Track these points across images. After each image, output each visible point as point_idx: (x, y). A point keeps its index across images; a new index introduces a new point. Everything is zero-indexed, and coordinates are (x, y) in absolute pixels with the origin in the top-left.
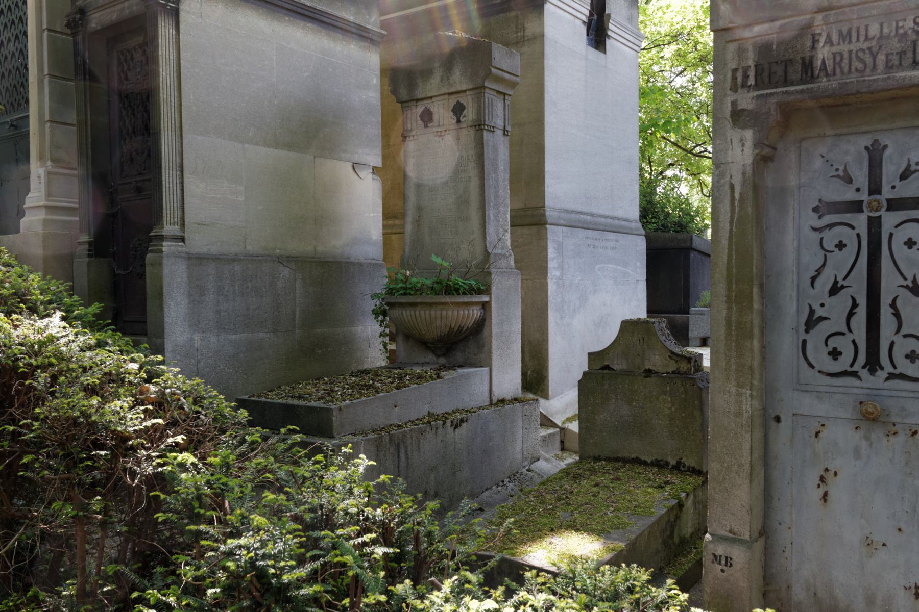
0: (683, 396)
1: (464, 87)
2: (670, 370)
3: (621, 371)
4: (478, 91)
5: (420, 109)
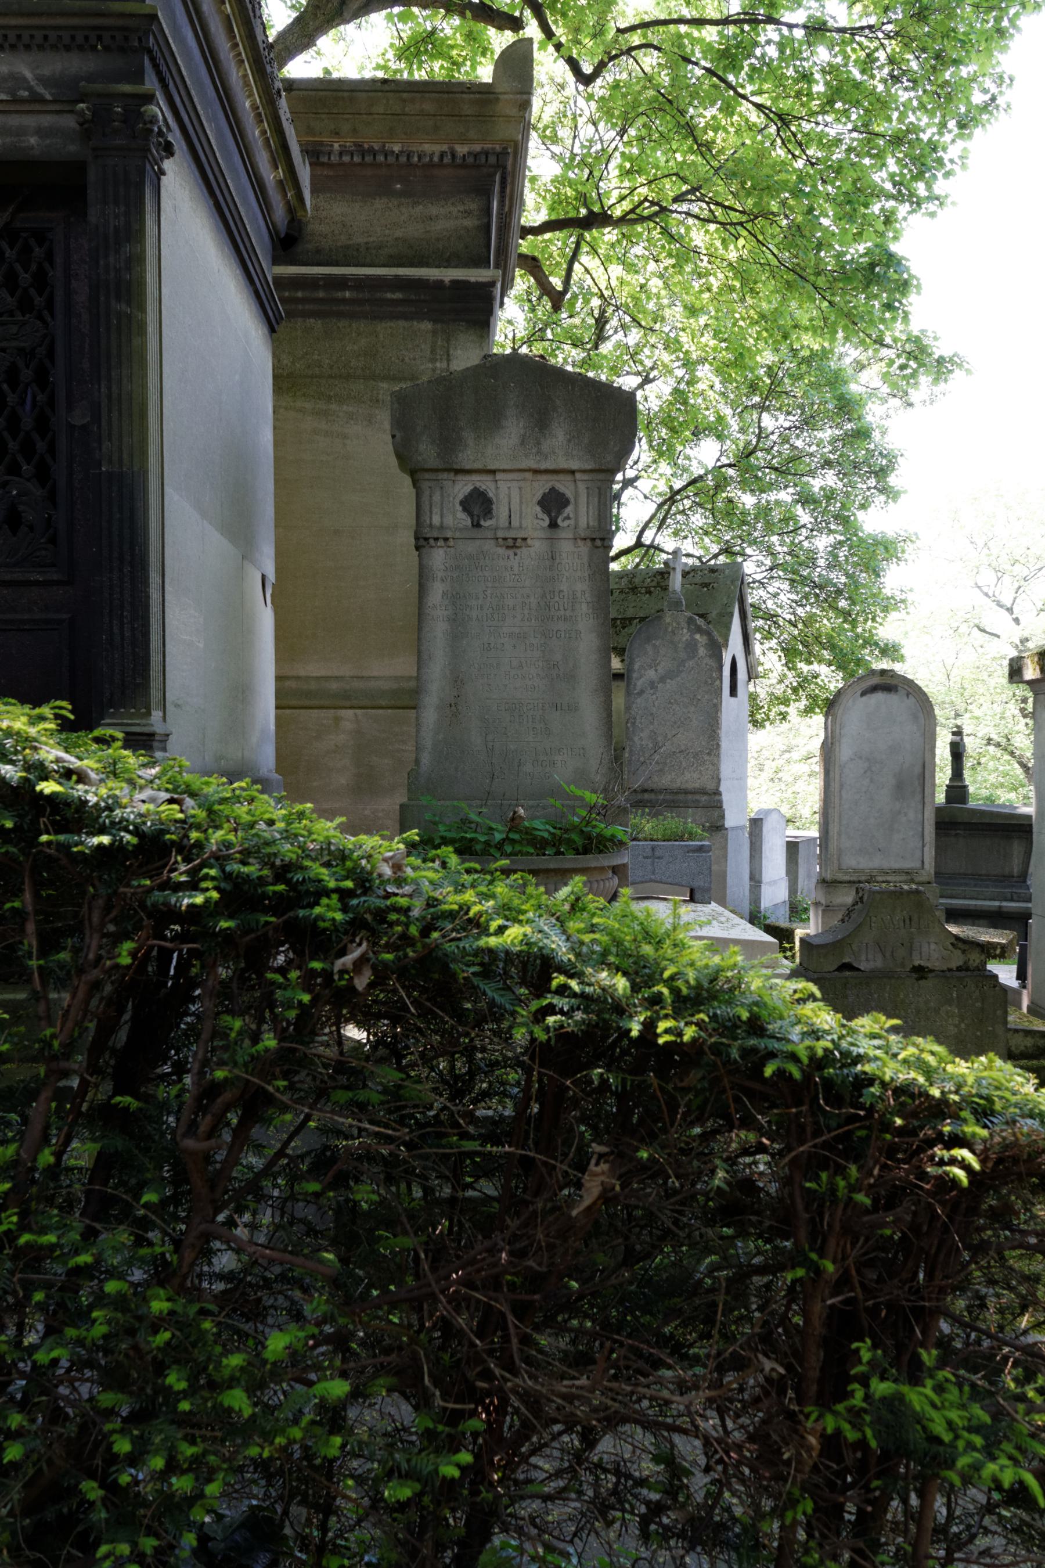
0: (978, 1005)
1: (574, 465)
2: (954, 965)
3: (872, 971)
4: (601, 476)
5: (463, 487)
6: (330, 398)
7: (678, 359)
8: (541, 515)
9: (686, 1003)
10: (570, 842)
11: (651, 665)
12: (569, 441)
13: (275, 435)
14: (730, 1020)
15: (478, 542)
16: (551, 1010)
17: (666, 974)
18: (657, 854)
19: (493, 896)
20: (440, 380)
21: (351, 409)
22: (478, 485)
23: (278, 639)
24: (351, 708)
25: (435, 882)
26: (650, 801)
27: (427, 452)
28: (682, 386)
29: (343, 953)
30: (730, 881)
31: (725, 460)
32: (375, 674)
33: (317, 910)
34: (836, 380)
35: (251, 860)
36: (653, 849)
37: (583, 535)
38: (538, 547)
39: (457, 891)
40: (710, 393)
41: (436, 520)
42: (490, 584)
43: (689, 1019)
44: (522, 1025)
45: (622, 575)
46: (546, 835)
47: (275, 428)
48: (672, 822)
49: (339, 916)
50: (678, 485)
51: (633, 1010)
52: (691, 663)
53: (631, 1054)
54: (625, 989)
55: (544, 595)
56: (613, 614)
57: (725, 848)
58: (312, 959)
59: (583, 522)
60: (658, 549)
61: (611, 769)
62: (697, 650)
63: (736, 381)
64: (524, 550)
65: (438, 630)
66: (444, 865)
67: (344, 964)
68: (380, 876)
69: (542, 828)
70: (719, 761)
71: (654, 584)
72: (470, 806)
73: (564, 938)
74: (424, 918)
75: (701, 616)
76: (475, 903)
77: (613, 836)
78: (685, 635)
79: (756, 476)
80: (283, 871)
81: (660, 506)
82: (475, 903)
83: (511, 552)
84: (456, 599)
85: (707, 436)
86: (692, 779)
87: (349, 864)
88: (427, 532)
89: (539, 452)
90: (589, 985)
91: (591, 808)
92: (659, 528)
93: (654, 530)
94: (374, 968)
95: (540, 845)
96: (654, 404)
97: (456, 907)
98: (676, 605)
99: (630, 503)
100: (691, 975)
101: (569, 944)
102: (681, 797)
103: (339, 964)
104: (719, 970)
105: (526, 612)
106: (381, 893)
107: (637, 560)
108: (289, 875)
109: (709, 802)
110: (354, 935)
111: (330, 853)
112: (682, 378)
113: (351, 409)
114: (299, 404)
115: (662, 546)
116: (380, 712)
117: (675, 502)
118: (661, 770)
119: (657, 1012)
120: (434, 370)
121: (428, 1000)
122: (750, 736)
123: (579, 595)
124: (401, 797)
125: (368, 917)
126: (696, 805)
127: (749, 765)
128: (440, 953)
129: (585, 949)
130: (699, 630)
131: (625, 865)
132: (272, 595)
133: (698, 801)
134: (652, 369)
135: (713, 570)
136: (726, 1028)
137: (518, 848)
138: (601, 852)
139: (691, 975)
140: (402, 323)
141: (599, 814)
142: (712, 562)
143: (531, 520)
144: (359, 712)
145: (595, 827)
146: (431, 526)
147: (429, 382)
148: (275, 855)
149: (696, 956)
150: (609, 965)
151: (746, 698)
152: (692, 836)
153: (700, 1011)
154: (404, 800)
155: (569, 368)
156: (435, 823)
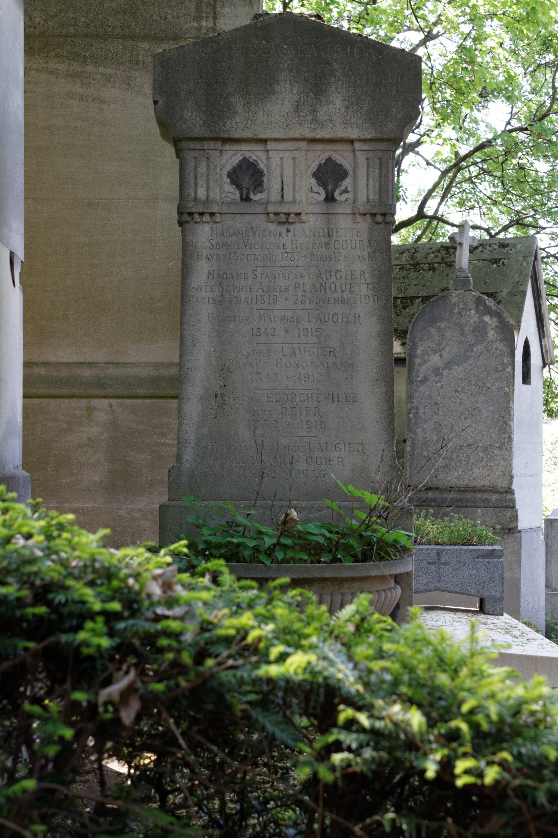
1: (353, 134)
4: (383, 146)
5: (231, 158)
6: (85, 58)
7: (464, 14)
8: (316, 188)
9: (488, 740)
10: (347, 547)
11: (435, 349)
12: (347, 107)
13: (26, 99)
14: (536, 759)
15: (247, 217)
16: (338, 747)
17: (465, 708)
18: (443, 559)
19: (272, 618)
20: (206, 42)
21: (108, 71)
22: (247, 155)
23: (28, 320)
24: (105, 397)
25: (211, 603)
26: (435, 500)
27: (192, 120)
28: (469, 43)
29: (108, 682)
30: (523, 589)
31: (515, 124)
32: (133, 359)
33: (82, 636)
35: (10, 579)
36: (438, 554)
37: (362, 210)
38: (313, 222)
39: (234, 614)
40: (500, 50)
41: (201, 193)
43: (491, 758)
44: (306, 763)
45: (402, 250)
46: (321, 540)
47: (25, 91)
48: (460, 524)
49: (105, 642)
50: (464, 150)
51: (427, 747)
52: (479, 348)
53: (422, 794)
54: (420, 726)
55: (319, 276)
56: (394, 293)
57: (518, 552)
58: (75, 688)
59: (362, 196)
60: (442, 220)
61: (393, 467)
62: (486, 333)
63: (528, 38)
64: (298, 226)
65: (203, 313)
66: (215, 581)
67: (110, 695)
68: (149, 596)
69: (316, 532)
70: (511, 456)
71: (438, 260)
72: (236, 507)
73: (351, 665)
74: (197, 643)
75: (491, 295)
76: (253, 628)
77: (395, 541)
78: (473, 317)
79: (550, 141)
80: (43, 592)
81: (444, 173)
82: (253, 628)
83: (283, 229)
84: (223, 279)
85: (497, 97)
86: (480, 476)
87: (115, 583)
88: (191, 206)
90: (381, 718)
91: (372, 511)
92: (443, 198)
93: (438, 200)
94: (142, 699)
95: (315, 551)
96: (438, 63)
97: (232, 632)
98: (463, 284)
99: (411, 170)
100: (493, 710)
101: (356, 673)
102: (469, 496)
103: (105, 694)
104: (521, 703)
105: (300, 294)
106: (150, 615)
107: (419, 232)
108: (51, 596)
109: (500, 501)
110: (121, 662)
111: (95, 571)
112: (469, 34)
113: (108, 71)
114: (51, 65)
115: (447, 217)
116: (138, 401)
117: (460, 169)
118: (447, 466)
119: (455, 750)
120: (199, 29)
121: (199, 732)
122: (545, 426)
123: (358, 276)
124: (161, 497)
125: (136, 642)
126: (486, 505)
127: (544, 458)
128: (215, 683)
129: (373, 678)
130: (488, 311)
131: (408, 574)
132: (21, 274)
133: (487, 500)
134: (435, 24)
135: (503, 245)
136: (530, 767)
137: (290, 554)
138: (382, 559)
139: (493, 710)
141: (379, 517)
142: (501, 236)
143: (306, 194)
144: (114, 401)
145: (375, 531)
146: (195, 199)
147: (195, 43)
148: (36, 574)
149: (497, 687)
150: (400, 696)
151: (541, 386)
152: (481, 540)
153: (502, 750)
154: (164, 499)
155: (345, 25)
156: (199, 527)
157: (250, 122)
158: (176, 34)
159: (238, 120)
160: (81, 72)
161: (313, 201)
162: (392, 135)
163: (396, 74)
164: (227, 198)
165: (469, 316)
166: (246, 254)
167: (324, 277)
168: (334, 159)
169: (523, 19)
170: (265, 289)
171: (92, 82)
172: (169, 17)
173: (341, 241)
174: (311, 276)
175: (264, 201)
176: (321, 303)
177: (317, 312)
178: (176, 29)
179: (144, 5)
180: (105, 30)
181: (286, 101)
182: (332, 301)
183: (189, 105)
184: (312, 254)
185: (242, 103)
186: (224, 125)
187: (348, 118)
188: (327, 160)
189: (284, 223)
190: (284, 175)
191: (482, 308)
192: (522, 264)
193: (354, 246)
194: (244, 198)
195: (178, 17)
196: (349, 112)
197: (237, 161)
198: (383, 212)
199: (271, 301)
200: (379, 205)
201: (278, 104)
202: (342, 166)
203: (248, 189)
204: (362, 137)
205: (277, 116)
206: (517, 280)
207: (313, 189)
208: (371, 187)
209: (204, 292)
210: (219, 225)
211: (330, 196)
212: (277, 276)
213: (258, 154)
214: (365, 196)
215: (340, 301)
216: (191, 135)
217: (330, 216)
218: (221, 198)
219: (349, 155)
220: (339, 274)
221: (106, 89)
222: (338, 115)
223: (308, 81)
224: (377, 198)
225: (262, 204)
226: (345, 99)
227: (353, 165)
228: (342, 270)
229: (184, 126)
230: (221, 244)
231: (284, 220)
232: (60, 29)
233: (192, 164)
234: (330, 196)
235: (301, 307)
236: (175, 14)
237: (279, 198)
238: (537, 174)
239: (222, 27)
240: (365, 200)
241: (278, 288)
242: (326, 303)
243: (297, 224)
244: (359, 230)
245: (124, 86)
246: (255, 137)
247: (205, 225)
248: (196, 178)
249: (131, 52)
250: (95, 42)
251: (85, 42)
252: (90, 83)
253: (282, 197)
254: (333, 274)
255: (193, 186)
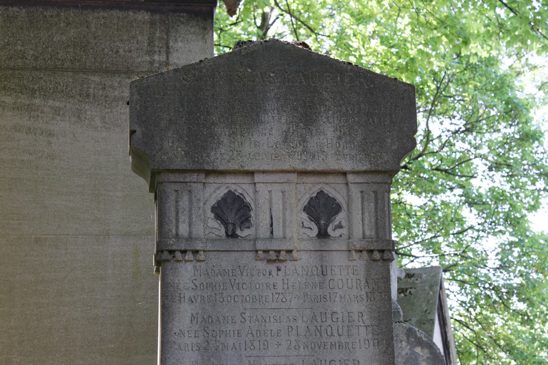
1: (347, 165)
4: (379, 178)
5: (214, 191)
6: (33, 91)
8: (308, 223)
12: (340, 138)
15: (234, 255)
21: (57, 104)
22: (233, 188)
34: (501, 87)
37: (358, 247)
38: (305, 260)
41: (184, 229)
42: (248, 306)
55: (314, 318)
59: (358, 232)
64: (289, 264)
83: (273, 267)
84: (208, 324)
88: (172, 244)
89: (305, 151)
105: (293, 338)
113: (57, 104)
120: (152, 63)
123: (356, 317)
140: (116, 13)
143: (297, 230)
157: (235, 153)
158: (128, 68)
159: (223, 151)
160: (29, 105)
161: (305, 237)
162: (387, 167)
163: (389, 104)
164: (211, 234)
165: (401, 347)
166: (233, 295)
167: (319, 320)
168: (326, 192)
169: (402, 68)
170: (254, 333)
171: (40, 115)
172: (121, 50)
173: (336, 280)
174: (305, 319)
175: (252, 237)
176: (317, 348)
177: (313, 358)
178: (128, 63)
179: (95, 38)
180: (55, 63)
181: (274, 131)
182: (329, 346)
183: (170, 135)
184: (305, 295)
185: (227, 133)
186: (208, 156)
187: (341, 149)
188: (318, 193)
189: (274, 261)
190: (273, 209)
191: (413, 340)
192: (428, 294)
193: (350, 286)
194: (230, 234)
195: (130, 51)
196: (341, 143)
197: (222, 195)
198: (380, 248)
199: (262, 347)
200: (376, 241)
201: (265, 134)
202: (335, 200)
203: (234, 225)
204: (356, 169)
205: (265, 147)
206: (425, 309)
207: (305, 224)
208: (366, 222)
209: (187, 337)
210: (202, 263)
211: (323, 232)
212: (268, 320)
213: (244, 186)
214: (361, 232)
215: (337, 345)
216: (172, 167)
217: (324, 253)
218: (205, 235)
219: (342, 189)
220: (335, 316)
221: (55, 122)
222: (330, 146)
223: (296, 110)
224: (373, 233)
225: (250, 240)
226: (336, 130)
227: (346, 198)
228: (339, 312)
229: (165, 158)
230: (205, 284)
231: (275, 258)
232: (7, 62)
233: (173, 198)
234: (323, 232)
235: (295, 353)
236: (127, 48)
237: (268, 234)
238: (411, 208)
239: (175, 61)
240: (361, 235)
241: (269, 333)
242: (322, 349)
243: (288, 262)
244: (355, 268)
245: (73, 119)
246: (242, 169)
247: (188, 263)
248: (177, 213)
249: (82, 85)
250: (44, 75)
251: (33, 75)
252: (38, 116)
253: (272, 233)
254: (329, 316)
255: (174, 221)
